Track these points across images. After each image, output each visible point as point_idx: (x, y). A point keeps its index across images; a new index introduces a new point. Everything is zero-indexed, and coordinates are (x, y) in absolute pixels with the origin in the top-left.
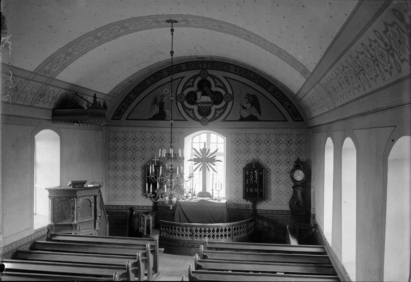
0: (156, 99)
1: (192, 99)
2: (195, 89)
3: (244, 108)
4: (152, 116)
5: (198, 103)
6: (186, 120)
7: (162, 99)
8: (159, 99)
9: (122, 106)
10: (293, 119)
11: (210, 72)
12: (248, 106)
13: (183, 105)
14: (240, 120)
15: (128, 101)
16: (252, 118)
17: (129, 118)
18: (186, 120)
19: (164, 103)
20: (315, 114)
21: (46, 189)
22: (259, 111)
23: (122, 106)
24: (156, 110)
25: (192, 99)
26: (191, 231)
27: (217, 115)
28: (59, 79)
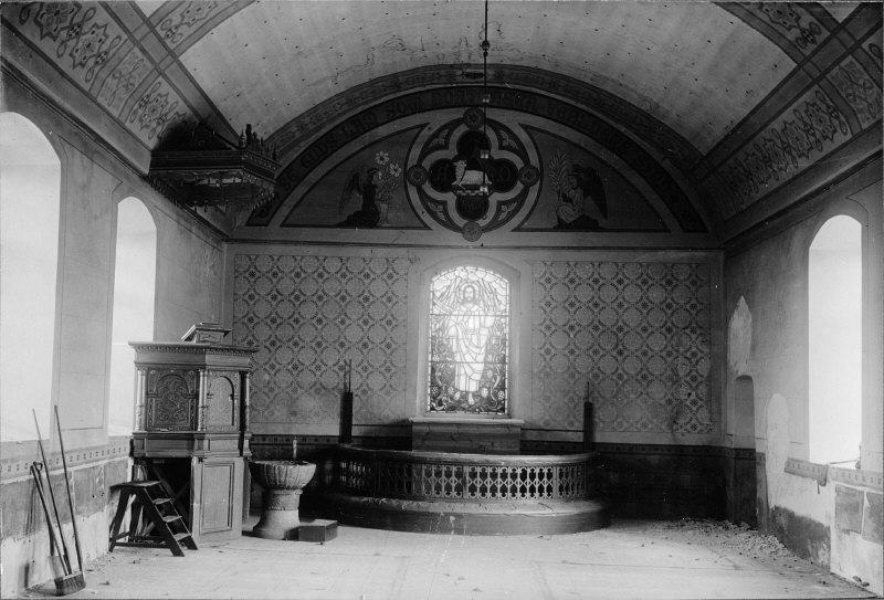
0: (356, 177)
1: (443, 176)
2: (451, 153)
3: (568, 200)
5: (458, 188)
6: (426, 227)
8: (364, 178)
10: (682, 227)
11: (492, 114)
12: (576, 195)
13: (421, 192)
14: (556, 229)
16: (583, 224)
18: (426, 227)
19: (376, 186)
22: (604, 210)
24: (357, 202)
25: (443, 176)
26: (459, 475)
27: (503, 216)
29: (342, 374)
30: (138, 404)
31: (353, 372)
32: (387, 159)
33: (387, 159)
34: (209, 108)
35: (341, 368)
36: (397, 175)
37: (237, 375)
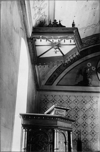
4: (77, 83)
7: (86, 70)
8: (83, 70)
9: (54, 75)
15: (59, 71)
17: (59, 84)
19: (87, 73)
20: (47, 14)
21: (20, 114)
23: (54, 75)
24: (81, 78)
28: (62, 54)
29: (77, 135)
30: (23, 147)
31: (81, 134)
32: (91, 65)
33: (91, 65)
34: (37, 45)
35: (77, 133)
36: (94, 70)
37: (67, 132)
